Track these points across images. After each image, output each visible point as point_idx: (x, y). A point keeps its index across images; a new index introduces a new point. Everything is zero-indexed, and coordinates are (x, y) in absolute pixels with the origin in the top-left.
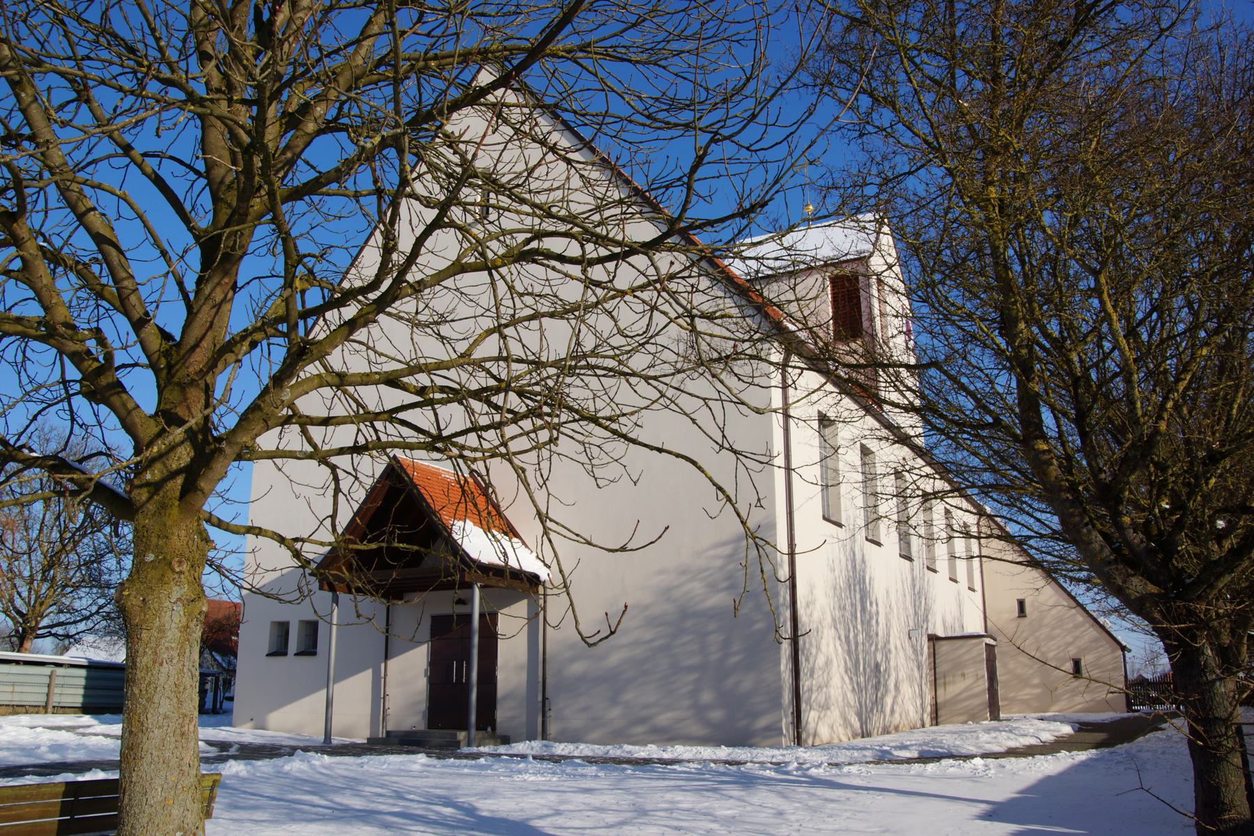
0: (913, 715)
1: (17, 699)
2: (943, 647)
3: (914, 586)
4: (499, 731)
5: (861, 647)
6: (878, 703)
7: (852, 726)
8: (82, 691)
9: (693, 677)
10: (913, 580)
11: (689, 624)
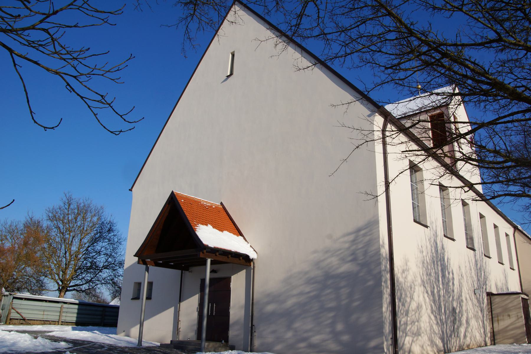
0: (479, 338)
1: (45, 318)
2: (493, 298)
3: (476, 264)
4: (230, 343)
5: (442, 298)
6: (455, 331)
7: (437, 346)
8: (75, 315)
9: (332, 314)
10: (476, 261)
11: (330, 282)
